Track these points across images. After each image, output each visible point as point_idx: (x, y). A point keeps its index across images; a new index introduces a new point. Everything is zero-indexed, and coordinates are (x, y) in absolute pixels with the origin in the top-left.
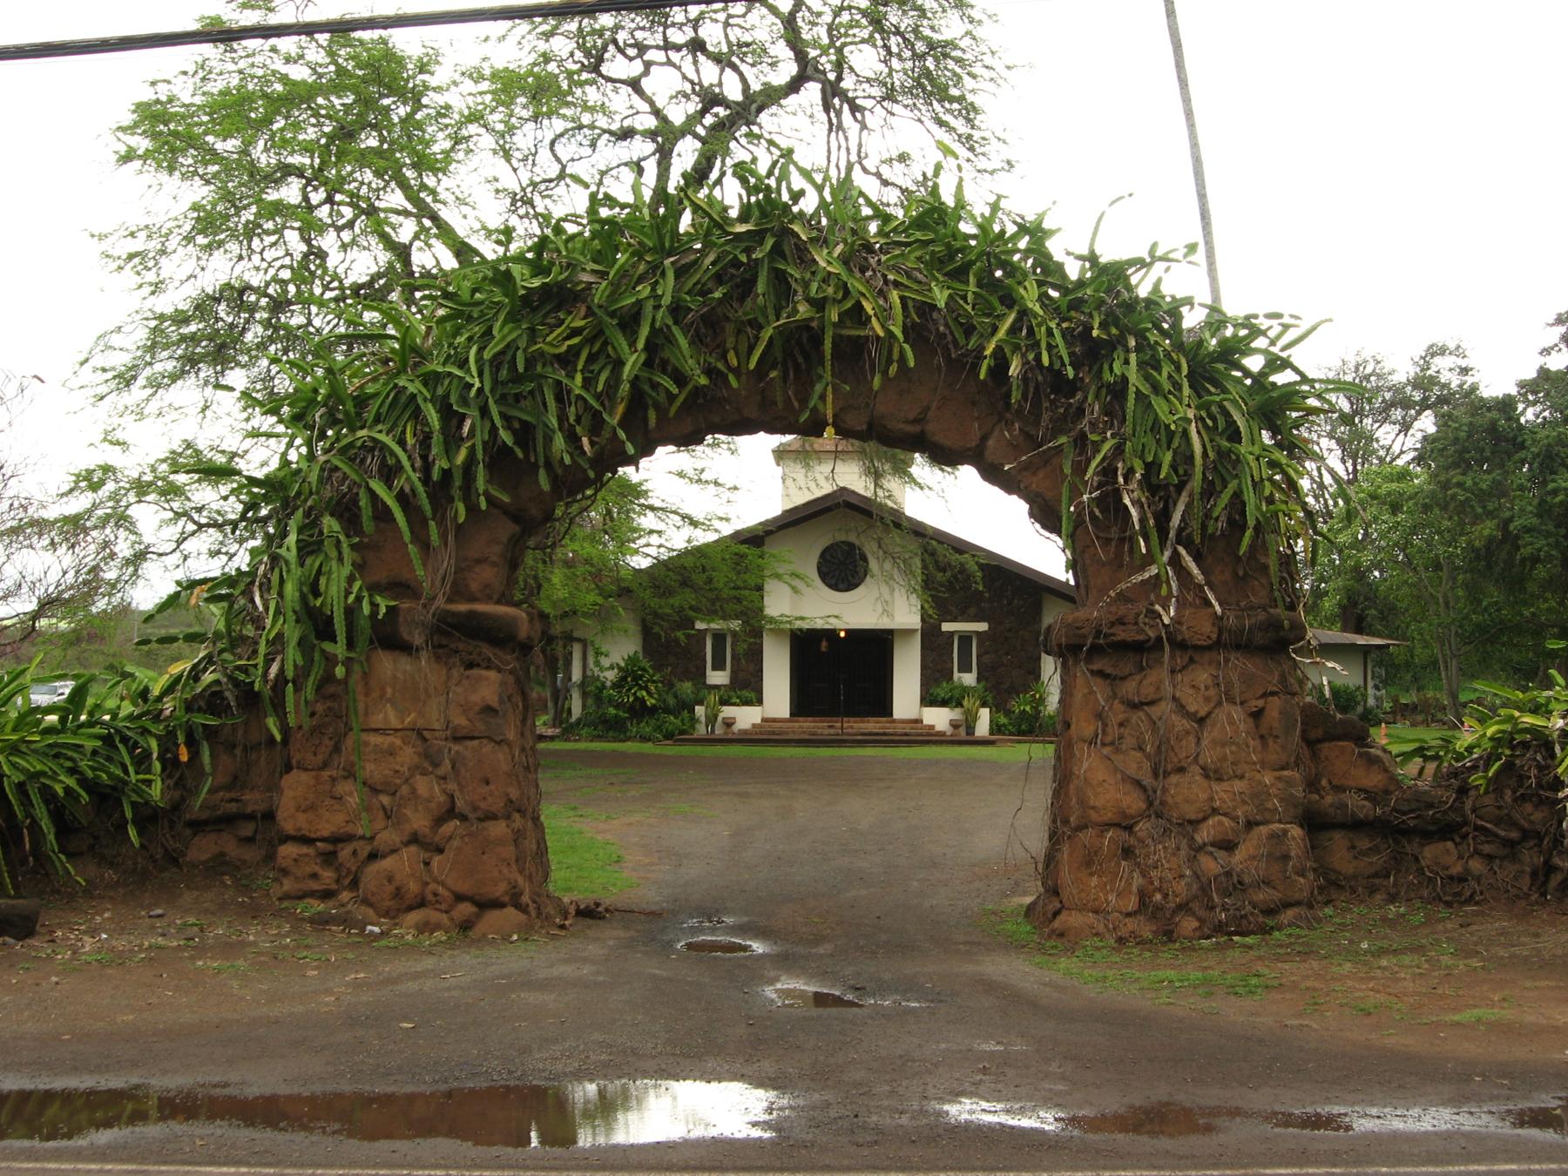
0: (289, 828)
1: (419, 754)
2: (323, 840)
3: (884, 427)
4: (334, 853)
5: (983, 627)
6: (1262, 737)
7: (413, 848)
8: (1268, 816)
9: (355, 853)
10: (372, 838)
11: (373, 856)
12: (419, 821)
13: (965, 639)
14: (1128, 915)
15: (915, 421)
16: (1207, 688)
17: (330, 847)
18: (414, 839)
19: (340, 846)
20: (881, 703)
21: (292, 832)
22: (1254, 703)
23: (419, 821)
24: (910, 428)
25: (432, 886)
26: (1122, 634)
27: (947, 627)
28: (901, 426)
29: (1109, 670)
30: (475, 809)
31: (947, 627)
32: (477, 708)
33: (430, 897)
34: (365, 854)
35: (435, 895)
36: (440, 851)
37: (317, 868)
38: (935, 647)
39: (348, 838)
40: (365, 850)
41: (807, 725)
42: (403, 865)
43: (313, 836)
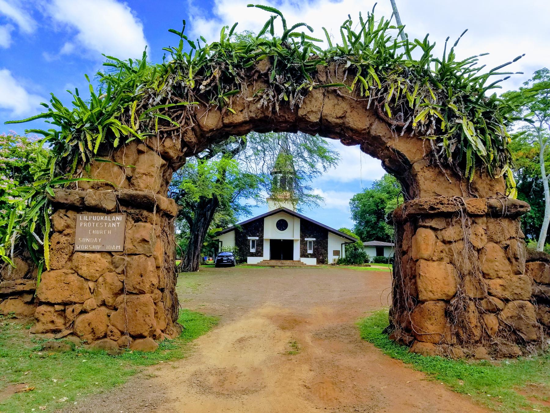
0: (42, 298)
1: (109, 262)
2: (59, 304)
3: (327, 120)
4: (64, 311)
5: (314, 239)
6: (509, 259)
7: (103, 308)
8: (516, 297)
9: (73, 311)
10: (83, 303)
11: (83, 312)
12: (105, 294)
13: (310, 242)
14: (119, 274)
15: (341, 118)
16: (482, 235)
17: (61, 308)
18: (104, 304)
19: (67, 307)
20: (291, 257)
21: (44, 301)
22: (504, 242)
23: (105, 294)
24: (338, 121)
25: (111, 327)
26: (443, 209)
27: (306, 239)
28: (335, 120)
29: (434, 226)
30: (135, 288)
31: (306, 239)
32: (138, 240)
33: (109, 333)
34: (79, 311)
35: (111, 332)
36: (116, 309)
37: (54, 319)
38: (303, 243)
39: (71, 303)
40: (78, 308)
41: (274, 262)
42: (99, 318)
43: (53, 302)
